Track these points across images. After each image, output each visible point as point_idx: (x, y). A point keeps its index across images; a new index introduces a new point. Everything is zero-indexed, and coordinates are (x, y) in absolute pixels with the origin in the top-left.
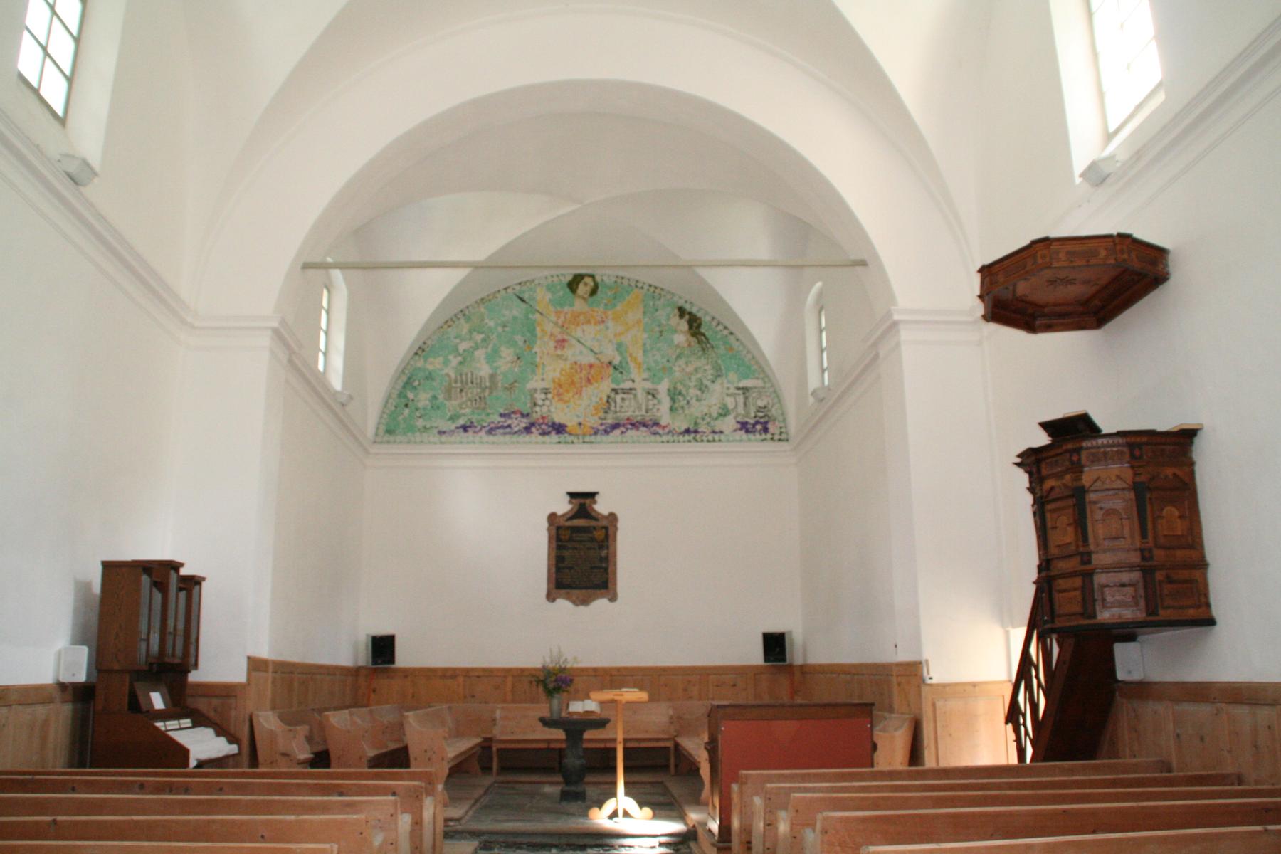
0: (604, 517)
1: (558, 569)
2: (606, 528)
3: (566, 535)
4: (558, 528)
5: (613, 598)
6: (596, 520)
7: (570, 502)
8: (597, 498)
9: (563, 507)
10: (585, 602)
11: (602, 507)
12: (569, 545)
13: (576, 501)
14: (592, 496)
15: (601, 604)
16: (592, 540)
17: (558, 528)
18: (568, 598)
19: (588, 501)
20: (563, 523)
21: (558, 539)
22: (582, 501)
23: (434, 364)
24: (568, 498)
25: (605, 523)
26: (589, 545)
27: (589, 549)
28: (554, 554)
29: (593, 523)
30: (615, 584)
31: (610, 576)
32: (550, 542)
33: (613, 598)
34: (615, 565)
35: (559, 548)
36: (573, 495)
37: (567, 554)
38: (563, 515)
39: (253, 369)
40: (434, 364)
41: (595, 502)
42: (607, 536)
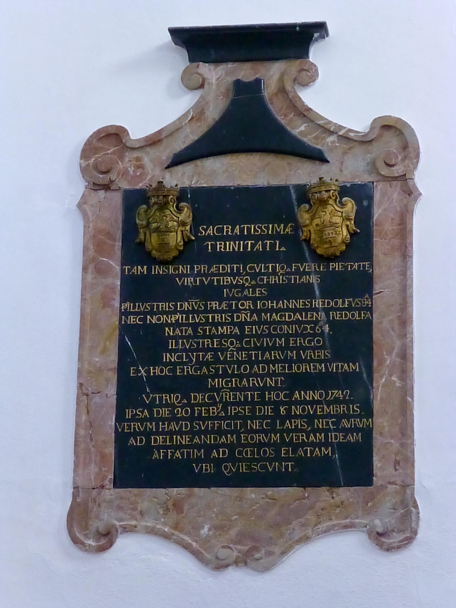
0: (347, 139)
1: (129, 393)
2: (361, 194)
3: (175, 227)
4: (134, 200)
5: (396, 533)
6: (318, 157)
7: (192, 83)
8: (316, 53)
9: (158, 103)
10: (255, 550)
11: (337, 94)
12: (188, 276)
13: (219, 76)
14: (293, 41)
15: (331, 561)
16: (297, 247)
17: (134, 200)
18: (177, 532)
19: (272, 74)
20: (152, 171)
21: (134, 249)
22: (245, 72)
23: (415, 161)
24: (180, 59)
25: (349, 168)
26: (277, 274)
27: (276, 292)
28: (111, 319)
29: (298, 174)
30: (405, 460)
31: (382, 423)
32: (92, 265)
33: (396, 533)
34: (87, 325)
35: (134, 289)
36: (200, 44)
37: (169, 316)
38: (154, 141)
39: (232, 185)
40: (415, 161)
41: (308, 76)
42: (361, 241)
